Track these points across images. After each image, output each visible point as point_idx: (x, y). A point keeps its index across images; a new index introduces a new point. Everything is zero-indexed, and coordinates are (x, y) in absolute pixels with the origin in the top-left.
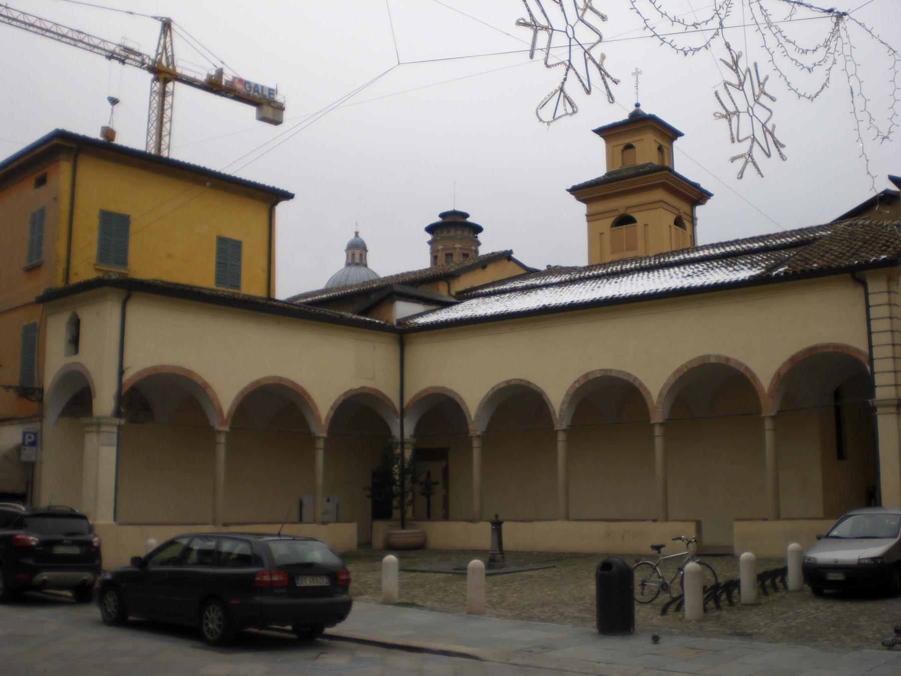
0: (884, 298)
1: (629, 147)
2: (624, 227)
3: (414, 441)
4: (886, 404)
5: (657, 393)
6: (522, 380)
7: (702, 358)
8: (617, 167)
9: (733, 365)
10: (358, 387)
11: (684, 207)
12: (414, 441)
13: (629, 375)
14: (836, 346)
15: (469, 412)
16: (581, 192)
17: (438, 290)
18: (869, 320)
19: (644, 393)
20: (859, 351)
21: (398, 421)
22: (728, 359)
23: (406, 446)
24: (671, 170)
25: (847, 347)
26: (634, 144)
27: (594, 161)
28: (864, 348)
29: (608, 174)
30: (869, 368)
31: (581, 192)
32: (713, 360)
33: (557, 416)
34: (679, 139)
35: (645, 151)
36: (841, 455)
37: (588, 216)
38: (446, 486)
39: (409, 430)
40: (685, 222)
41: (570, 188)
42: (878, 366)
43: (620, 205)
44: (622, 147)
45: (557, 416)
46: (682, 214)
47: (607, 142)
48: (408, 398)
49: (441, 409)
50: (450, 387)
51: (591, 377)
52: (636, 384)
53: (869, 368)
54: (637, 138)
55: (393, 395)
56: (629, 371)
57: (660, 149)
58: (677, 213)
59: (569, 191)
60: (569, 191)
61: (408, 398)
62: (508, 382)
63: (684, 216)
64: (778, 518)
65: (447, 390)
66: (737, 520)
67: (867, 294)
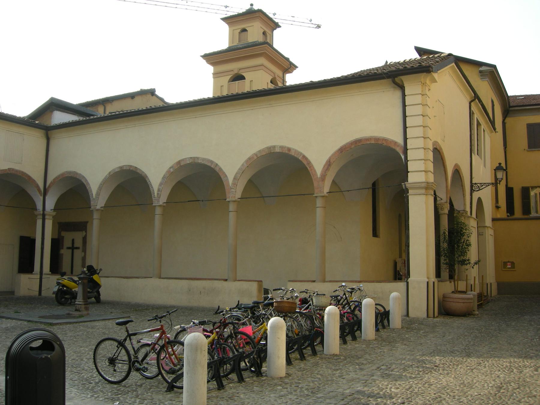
0: (419, 99)
1: (244, 30)
2: (237, 82)
3: (54, 214)
4: (417, 186)
5: (233, 177)
6: (131, 166)
7: (269, 148)
8: (236, 43)
9: (293, 154)
10: (6, 168)
11: (279, 72)
12: (54, 214)
13: (212, 162)
14: (377, 139)
15: (91, 191)
16: (212, 58)
17: (98, 111)
18: (404, 106)
19: (222, 177)
20: (395, 143)
21: (42, 198)
22: (289, 149)
23: (47, 217)
24: (271, 46)
25: (386, 140)
26: (247, 29)
27: (221, 39)
28: (401, 141)
29: (229, 48)
30: (403, 157)
31: (212, 58)
32: (278, 150)
33: (156, 194)
34: (278, 29)
35: (255, 33)
36: (375, 234)
37: (214, 74)
38: (84, 251)
39: (50, 204)
40: (278, 82)
41: (203, 54)
42: (411, 155)
43: (235, 67)
44: (239, 31)
45: (156, 194)
46: (276, 77)
47: (229, 27)
48: (51, 178)
49: (75, 190)
50: (79, 172)
51: (182, 164)
52: (217, 169)
53: (403, 157)
54: (250, 25)
55: (37, 176)
56: (211, 158)
57: (264, 33)
58: (273, 75)
59: (202, 56)
60: (202, 56)
61: (51, 178)
62: (121, 167)
63: (277, 78)
64: (324, 281)
65: (77, 173)
66: (289, 281)
67: (404, 96)
